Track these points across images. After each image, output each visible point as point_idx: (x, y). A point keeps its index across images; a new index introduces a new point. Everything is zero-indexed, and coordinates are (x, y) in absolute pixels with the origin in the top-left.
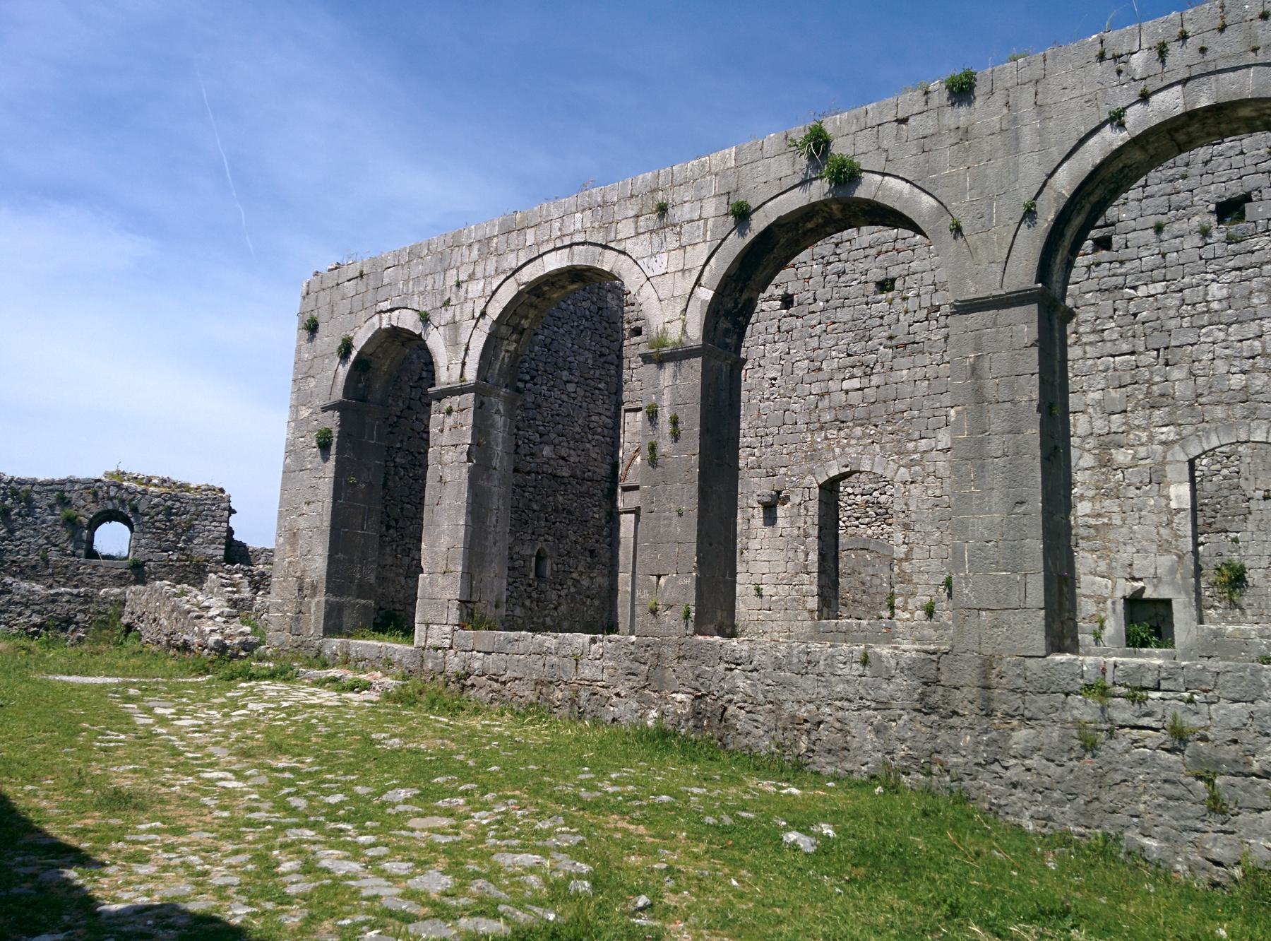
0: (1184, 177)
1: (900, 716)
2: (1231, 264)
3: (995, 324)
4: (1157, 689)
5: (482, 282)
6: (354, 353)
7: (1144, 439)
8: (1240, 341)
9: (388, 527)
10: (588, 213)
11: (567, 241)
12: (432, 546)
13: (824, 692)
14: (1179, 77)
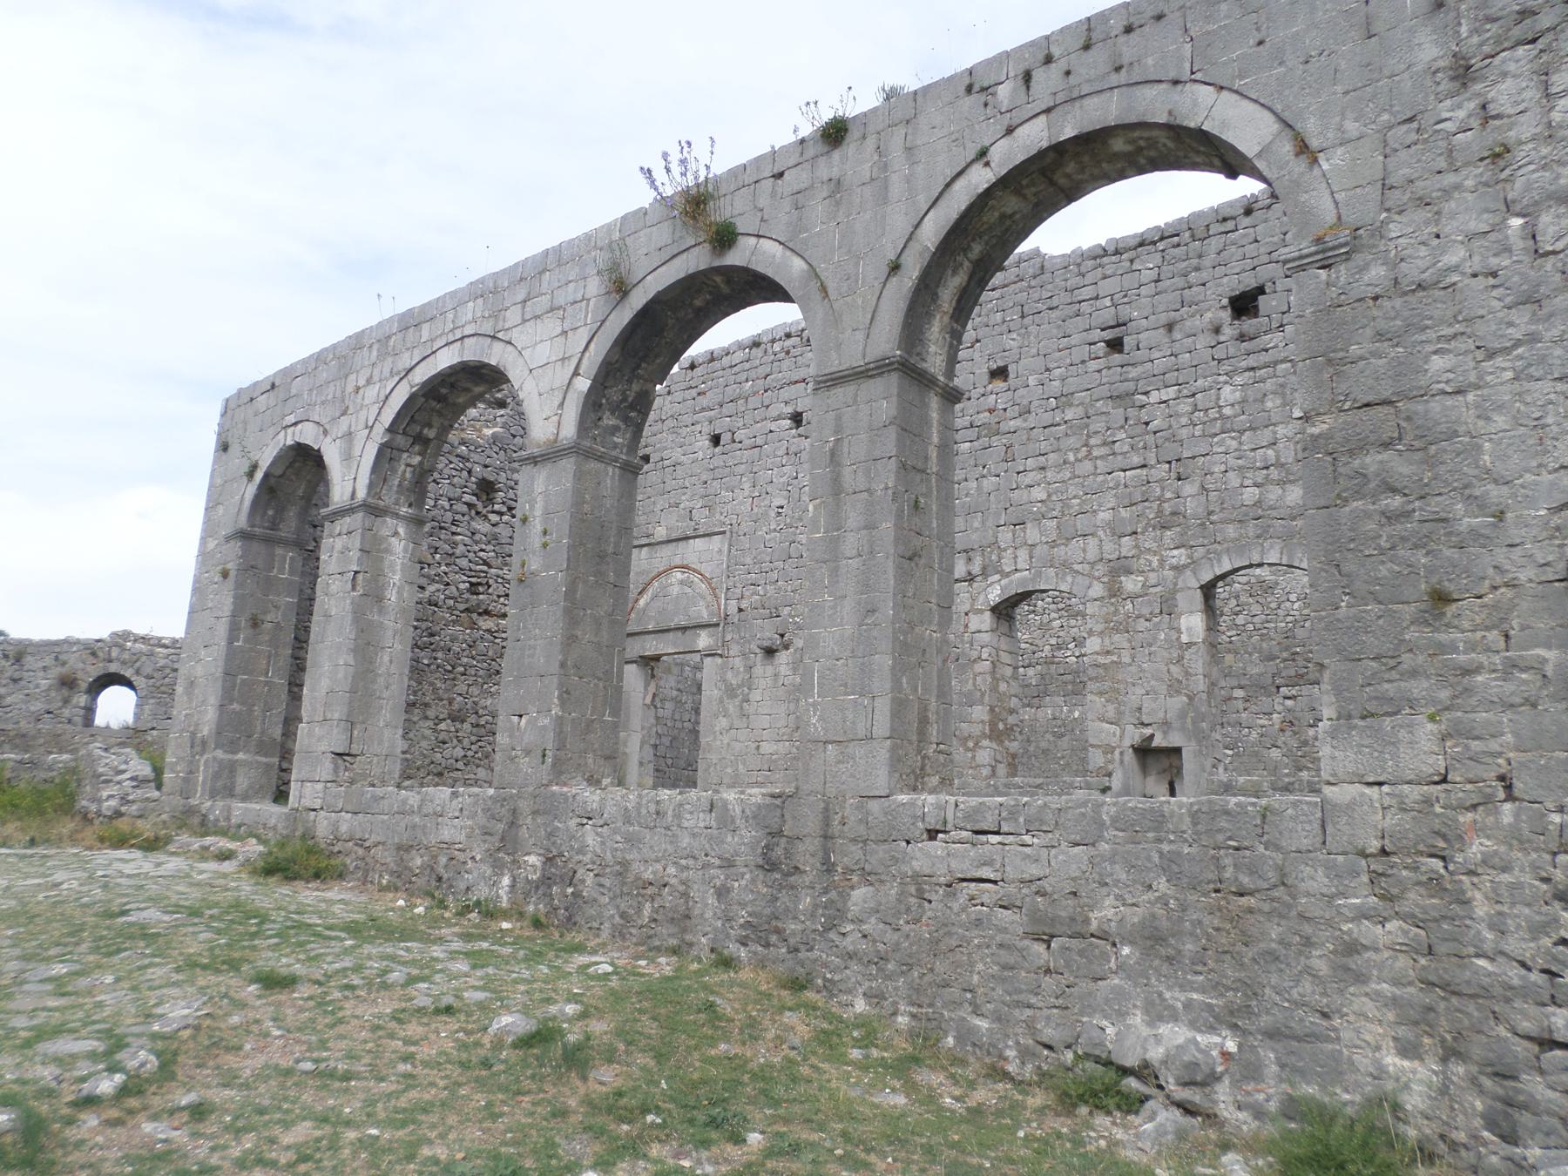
0: (1197, 269)
1: (743, 875)
2: (1244, 364)
3: (855, 401)
4: (997, 833)
7: (1155, 564)
8: (1254, 450)
10: (480, 301)
12: (312, 690)
13: (670, 849)
14: (1044, 107)
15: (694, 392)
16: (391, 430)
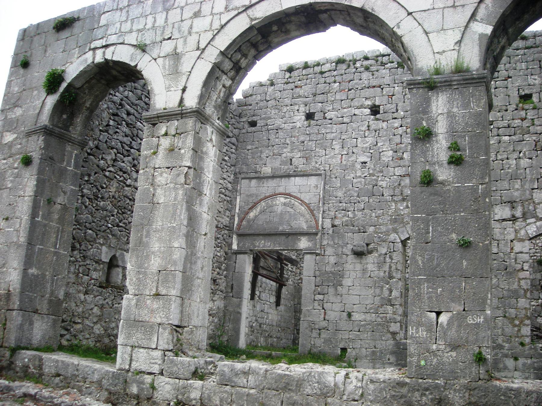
5: (209, 19)
6: (64, 85)
15: (292, 86)
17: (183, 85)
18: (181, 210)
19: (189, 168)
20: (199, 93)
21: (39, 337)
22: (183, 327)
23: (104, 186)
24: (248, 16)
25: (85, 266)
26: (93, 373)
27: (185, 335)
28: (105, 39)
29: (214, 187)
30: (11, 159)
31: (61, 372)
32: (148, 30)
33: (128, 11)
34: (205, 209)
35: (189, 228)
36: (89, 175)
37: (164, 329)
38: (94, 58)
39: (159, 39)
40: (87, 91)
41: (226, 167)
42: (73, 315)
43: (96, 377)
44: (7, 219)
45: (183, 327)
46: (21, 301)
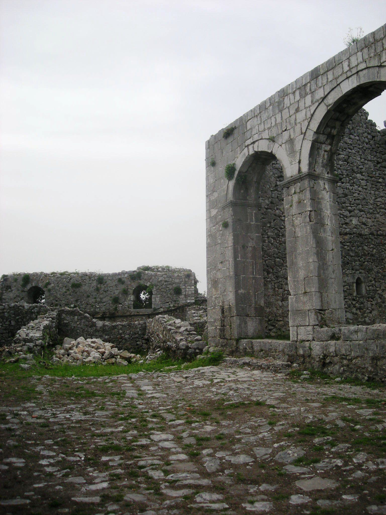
5: (304, 112)
6: (236, 173)
9: (268, 273)
11: (354, 71)
16: (317, 132)
17: (298, 158)
18: (310, 239)
19: (310, 211)
20: (308, 162)
21: (252, 331)
22: (325, 310)
23: (282, 227)
24: (325, 104)
25: (279, 282)
26: (279, 346)
27: (327, 314)
28: (252, 138)
29: (333, 218)
30: (217, 225)
31: (263, 348)
32: (273, 127)
33: (260, 117)
34: (329, 233)
35: (318, 249)
36: (270, 223)
37: (311, 313)
38: (249, 152)
39: (280, 132)
40: (251, 172)
41: (381, 187)
42: (276, 316)
43: (281, 348)
44: (222, 263)
45: (325, 310)
46: (237, 310)
